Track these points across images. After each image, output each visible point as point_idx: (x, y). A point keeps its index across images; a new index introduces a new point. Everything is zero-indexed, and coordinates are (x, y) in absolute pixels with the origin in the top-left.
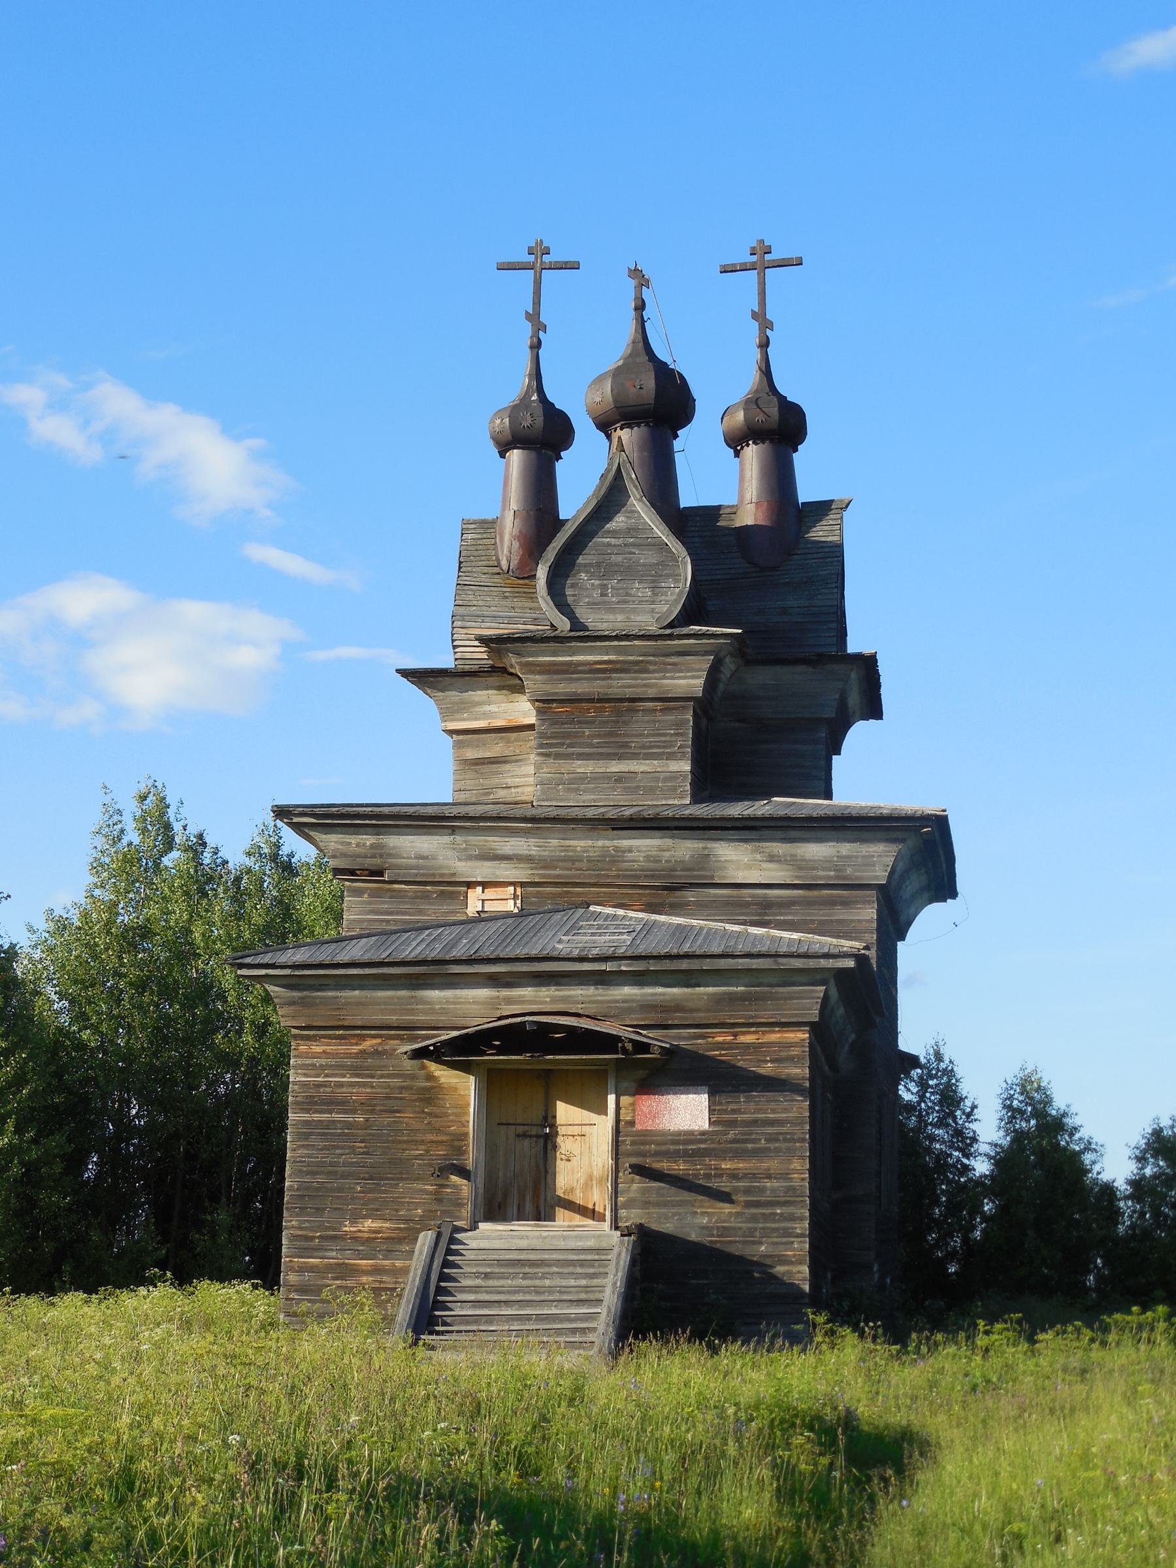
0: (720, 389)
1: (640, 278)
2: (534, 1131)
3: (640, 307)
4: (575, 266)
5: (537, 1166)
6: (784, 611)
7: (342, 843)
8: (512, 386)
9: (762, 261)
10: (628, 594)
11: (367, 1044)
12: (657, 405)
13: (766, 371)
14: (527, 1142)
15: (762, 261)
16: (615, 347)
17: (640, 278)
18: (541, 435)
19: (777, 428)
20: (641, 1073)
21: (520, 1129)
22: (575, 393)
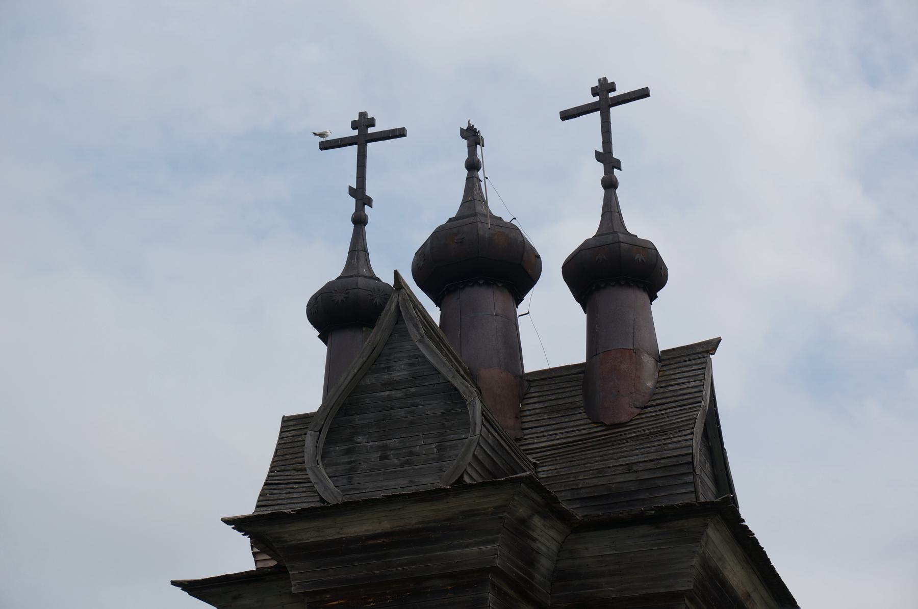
0: (558, 231)
1: (472, 136)
3: (473, 166)
8: (330, 266)
10: (411, 454)
12: (479, 260)
16: (446, 205)
18: (342, 311)
19: (617, 272)
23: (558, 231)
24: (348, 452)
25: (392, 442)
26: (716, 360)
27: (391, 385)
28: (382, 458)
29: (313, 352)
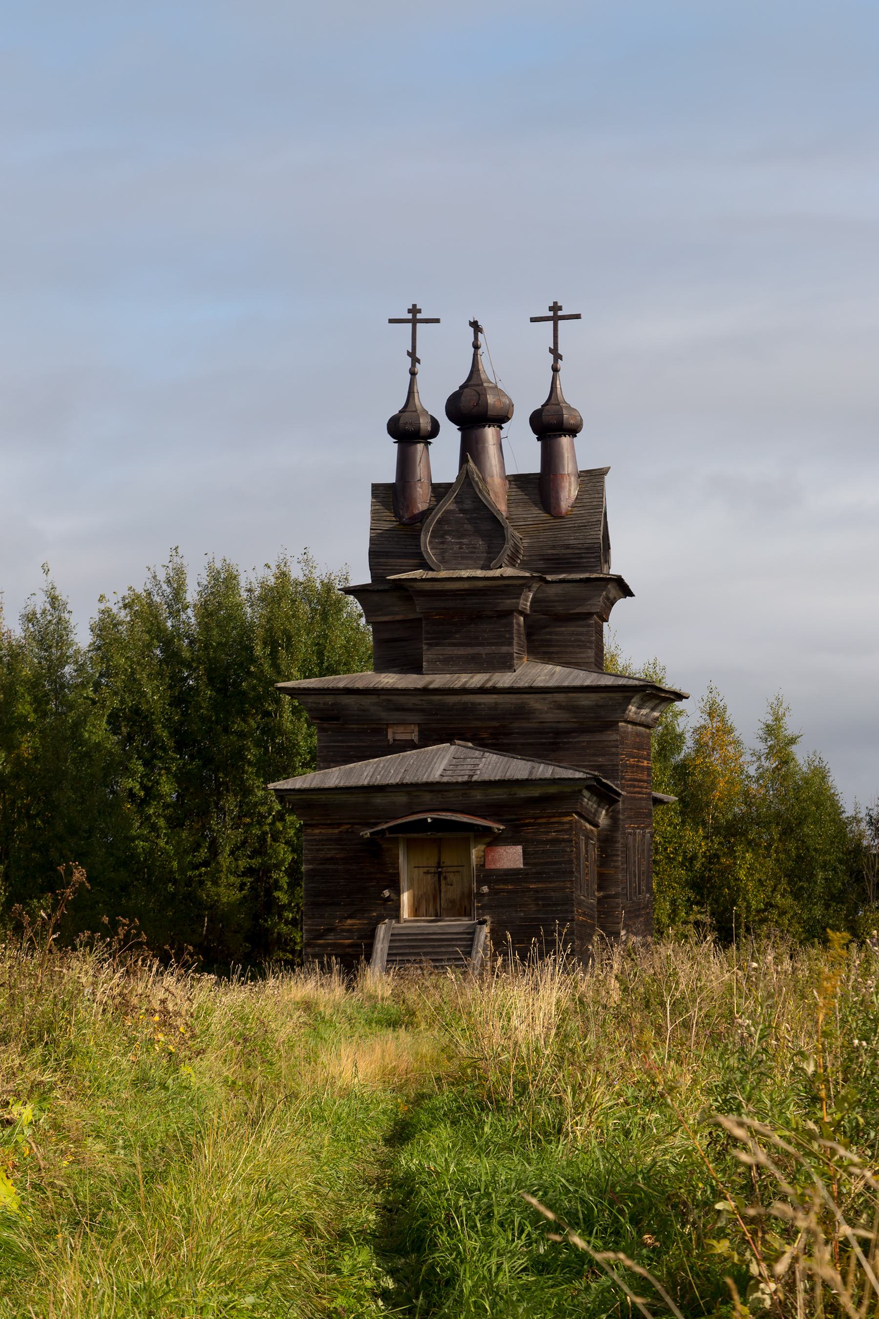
1: (475, 325)
2: (432, 870)
4: (437, 321)
5: (435, 888)
6: (567, 547)
7: (315, 703)
9: (556, 315)
11: (343, 828)
12: (474, 412)
14: (429, 876)
15: (556, 315)
17: (475, 325)
18: (408, 432)
19: (552, 425)
20: (488, 840)
21: (425, 869)
22: (434, 403)
23: (526, 400)
24: (442, 543)
25: (465, 541)
26: (607, 478)
28: (460, 548)
29: (391, 448)
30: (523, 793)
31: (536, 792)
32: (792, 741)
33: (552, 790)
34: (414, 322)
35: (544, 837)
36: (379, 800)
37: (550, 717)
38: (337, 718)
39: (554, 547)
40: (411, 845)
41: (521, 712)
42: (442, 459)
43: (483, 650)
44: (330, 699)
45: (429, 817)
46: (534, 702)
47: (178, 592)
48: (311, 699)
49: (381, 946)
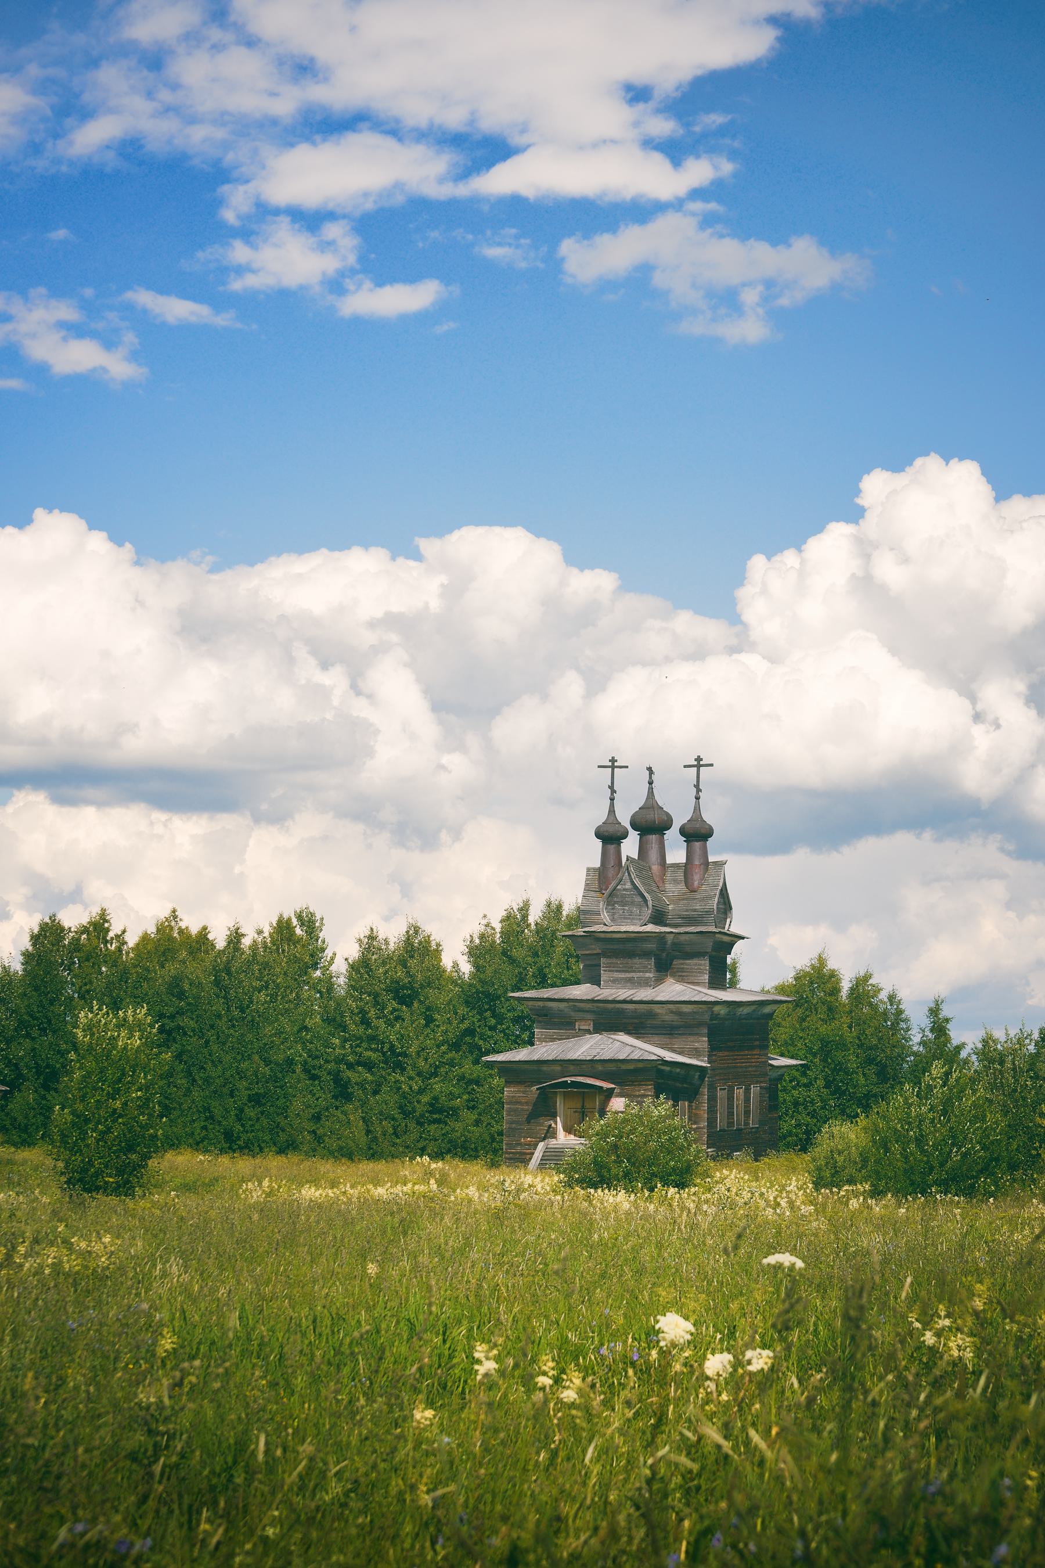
1: (650, 769)
6: (695, 910)
8: (600, 817)
12: (651, 825)
13: (697, 809)
17: (650, 769)
18: (610, 837)
23: (681, 818)
27: (625, 890)
30: (624, 1067)
31: (631, 1067)
32: (947, 1020)
33: (640, 1065)
34: (613, 767)
35: (637, 1093)
36: (545, 1068)
37: (667, 1018)
38: (546, 1015)
39: (687, 911)
40: (566, 1095)
41: (651, 1015)
42: (630, 847)
43: (635, 975)
44: (541, 1004)
45: (569, 1079)
46: (657, 1009)
47: (525, 917)
48: (531, 1003)
49: (538, 1154)
